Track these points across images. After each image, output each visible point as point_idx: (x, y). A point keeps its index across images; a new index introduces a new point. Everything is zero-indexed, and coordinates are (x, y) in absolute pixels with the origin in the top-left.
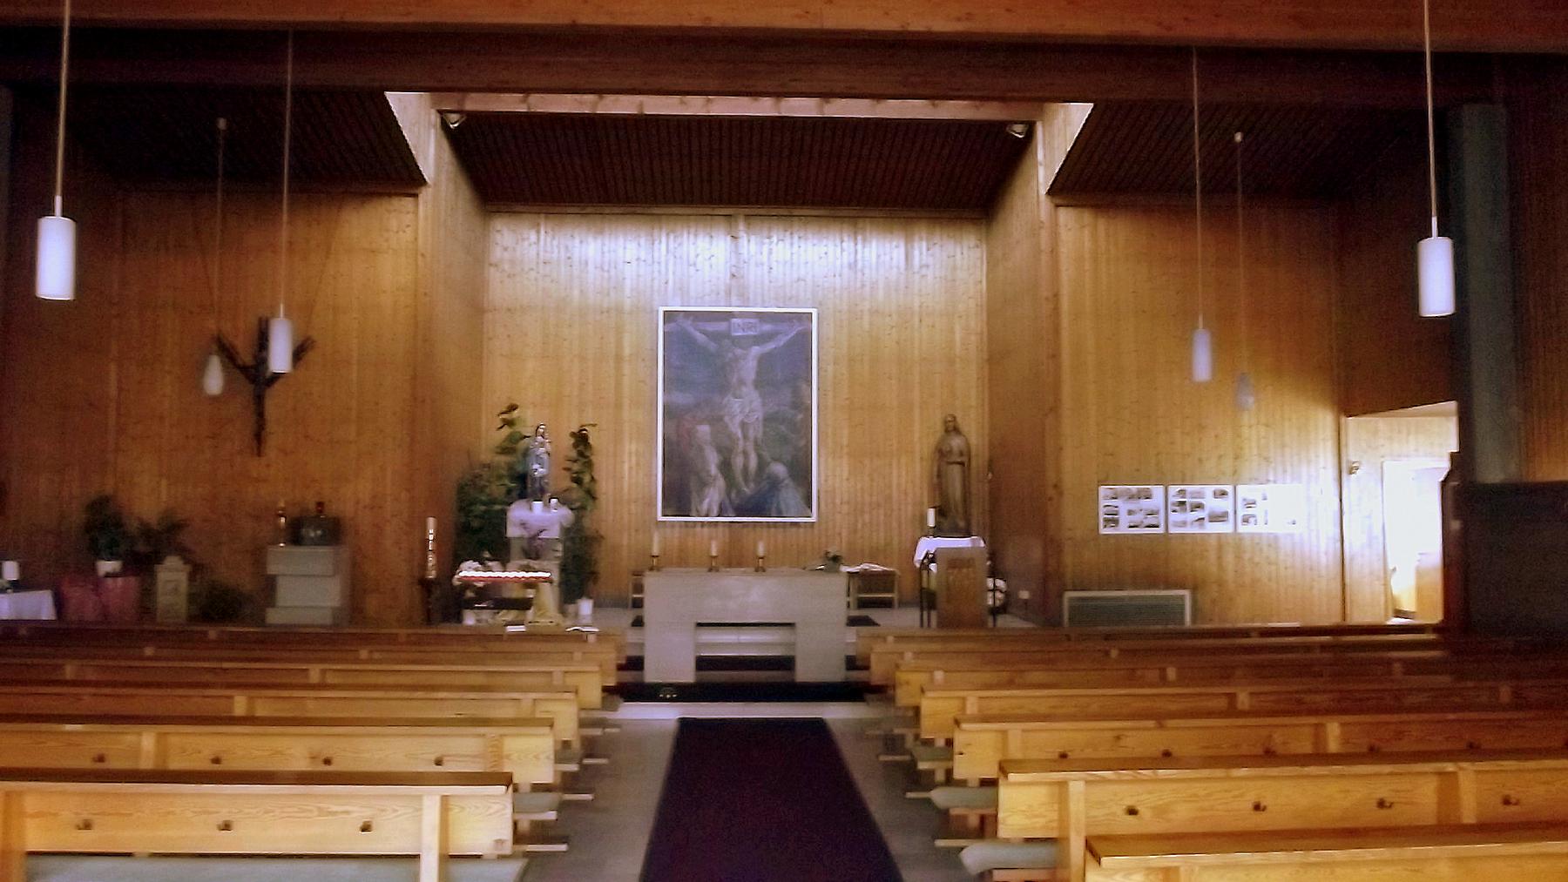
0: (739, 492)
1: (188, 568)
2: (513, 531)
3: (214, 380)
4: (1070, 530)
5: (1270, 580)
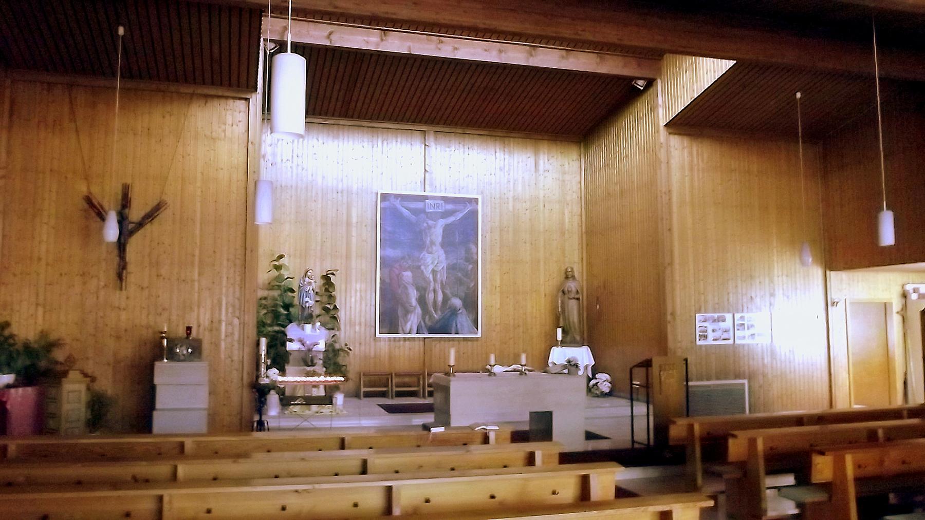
0: (431, 317)
4: (680, 342)
5: (790, 372)
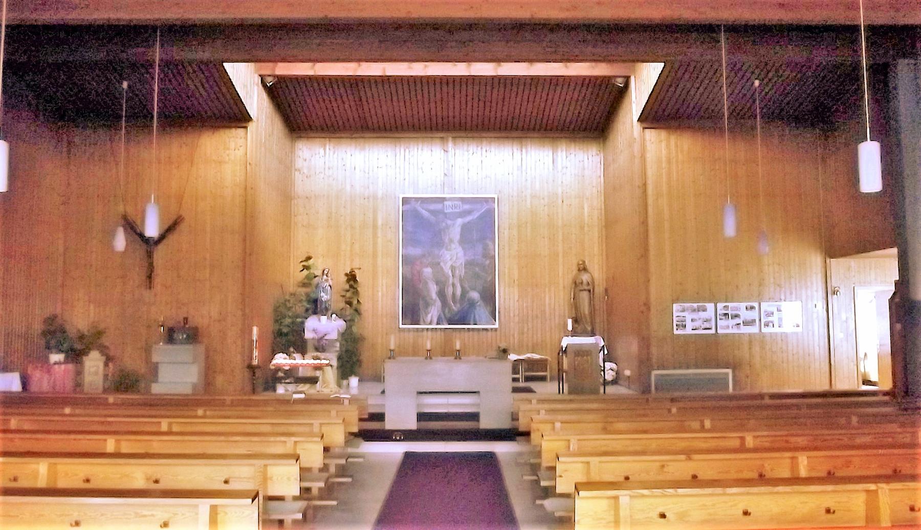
0: (450, 309)
1: (104, 358)
2: (308, 335)
3: (120, 241)
